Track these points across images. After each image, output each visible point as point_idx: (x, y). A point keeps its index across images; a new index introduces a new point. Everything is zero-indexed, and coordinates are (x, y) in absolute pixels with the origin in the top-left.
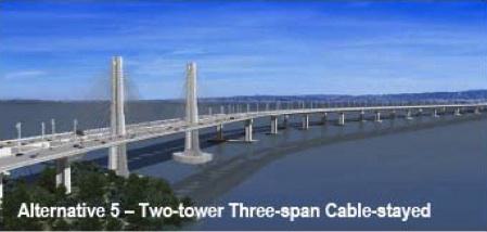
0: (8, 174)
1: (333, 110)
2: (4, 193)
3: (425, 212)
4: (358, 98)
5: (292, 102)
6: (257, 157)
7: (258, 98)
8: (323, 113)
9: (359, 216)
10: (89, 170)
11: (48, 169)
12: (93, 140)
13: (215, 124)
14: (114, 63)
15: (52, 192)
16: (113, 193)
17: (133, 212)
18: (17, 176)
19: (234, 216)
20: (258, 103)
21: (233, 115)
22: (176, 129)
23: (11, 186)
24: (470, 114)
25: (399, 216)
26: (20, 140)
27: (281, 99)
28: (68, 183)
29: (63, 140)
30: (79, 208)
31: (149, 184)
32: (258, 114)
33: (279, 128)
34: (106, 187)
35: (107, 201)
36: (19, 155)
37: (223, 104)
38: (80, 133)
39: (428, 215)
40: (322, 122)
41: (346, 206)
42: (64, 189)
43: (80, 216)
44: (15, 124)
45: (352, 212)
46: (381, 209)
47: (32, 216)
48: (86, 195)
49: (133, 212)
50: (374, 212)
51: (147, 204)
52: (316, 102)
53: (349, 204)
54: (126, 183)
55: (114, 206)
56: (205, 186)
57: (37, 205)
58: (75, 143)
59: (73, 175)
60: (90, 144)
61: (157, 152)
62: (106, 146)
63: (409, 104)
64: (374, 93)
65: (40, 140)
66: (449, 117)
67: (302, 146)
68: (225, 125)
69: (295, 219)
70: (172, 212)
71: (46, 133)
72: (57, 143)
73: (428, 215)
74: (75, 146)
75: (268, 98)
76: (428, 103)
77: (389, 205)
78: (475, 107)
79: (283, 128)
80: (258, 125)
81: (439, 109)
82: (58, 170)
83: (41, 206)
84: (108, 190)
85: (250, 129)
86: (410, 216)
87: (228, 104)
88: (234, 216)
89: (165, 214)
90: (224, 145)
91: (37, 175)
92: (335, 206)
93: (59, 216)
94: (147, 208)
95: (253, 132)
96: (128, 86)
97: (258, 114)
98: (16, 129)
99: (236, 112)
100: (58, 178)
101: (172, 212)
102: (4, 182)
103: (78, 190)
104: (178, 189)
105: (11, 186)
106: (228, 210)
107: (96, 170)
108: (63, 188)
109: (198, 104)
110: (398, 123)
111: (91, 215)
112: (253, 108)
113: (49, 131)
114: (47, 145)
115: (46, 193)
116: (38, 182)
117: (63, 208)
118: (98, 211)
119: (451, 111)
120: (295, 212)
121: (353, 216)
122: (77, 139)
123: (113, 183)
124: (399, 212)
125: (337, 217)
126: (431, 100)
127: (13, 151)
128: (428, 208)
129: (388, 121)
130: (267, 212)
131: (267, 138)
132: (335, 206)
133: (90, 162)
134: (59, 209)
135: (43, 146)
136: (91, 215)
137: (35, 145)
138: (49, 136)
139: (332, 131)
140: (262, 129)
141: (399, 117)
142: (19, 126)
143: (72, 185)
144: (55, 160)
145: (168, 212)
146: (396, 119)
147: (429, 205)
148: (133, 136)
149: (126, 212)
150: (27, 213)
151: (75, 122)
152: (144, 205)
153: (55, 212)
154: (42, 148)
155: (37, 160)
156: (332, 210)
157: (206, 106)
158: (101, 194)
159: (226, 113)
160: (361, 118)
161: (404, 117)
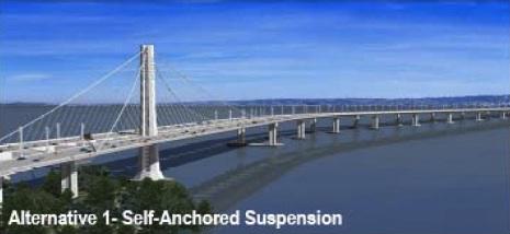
0: (8, 178)
2: (4, 197)
3: (234, 219)
4: (395, 101)
6: (282, 161)
8: (355, 116)
9: (215, 223)
10: (98, 174)
11: (52, 173)
12: (108, 143)
13: (236, 128)
15: (58, 196)
16: (124, 196)
18: (19, 181)
20: (283, 106)
21: (256, 119)
23: (12, 191)
24: (496, 120)
29: (70, 144)
30: (70, 215)
32: (283, 117)
33: (380, 125)
35: (118, 206)
36: (21, 159)
38: (88, 137)
40: (353, 126)
46: (312, 217)
47: (23, 223)
48: (94, 199)
53: (194, 212)
56: (152, 196)
58: (84, 146)
61: (172, 156)
63: (451, 108)
65: (44, 145)
66: (468, 124)
67: (332, 150)
69: (281, 226)
71: (51, 137)
72: (63, 147)
73: (237, 223)
74: (83, 150)
75: (294, 101)
76: (471, 107)
79: (310, 132)
82: (64, 173)
83: (32, 213)
84: (118, 194)
85: (273, 134)
87: (258, 108)
90: (244, 149)
91: (39, 179)
93: (49, 223)
95: (278, 137)
97: (283, 117)
99: (259, 115)
100: (64, 183)
102: (4, 187)
104: (196, 193)
105: (12, 191)
107: (105, 174)
108: (69, 192)
109: (159, 108)
110: (439, 127)
111: (83, 222)
112: (278, 111)
114: (52, 149)
115: (51, 198)
116: (40, 189)
117: (54, 216)
122: (85, 144)
123: (124, 188)
126: (475, 104)
127: (14, 155)
130: (289, 219)
131: (294, 142)
133: (100, 166)
134: (50, 216)
138: (53, 140)
139: (364, 135)
140: (287, 133)
141: (493, 116)
143: (80, 190)
144: (62, 165)
145: (208, 219)
146: (436, 123)
147: (238, 212)
148: (204, 131)
150: (17, 221)
151: (83, 127)
154: (49, 151)
157: (168, 113)
158: (111, 198)
160: (432, 120)
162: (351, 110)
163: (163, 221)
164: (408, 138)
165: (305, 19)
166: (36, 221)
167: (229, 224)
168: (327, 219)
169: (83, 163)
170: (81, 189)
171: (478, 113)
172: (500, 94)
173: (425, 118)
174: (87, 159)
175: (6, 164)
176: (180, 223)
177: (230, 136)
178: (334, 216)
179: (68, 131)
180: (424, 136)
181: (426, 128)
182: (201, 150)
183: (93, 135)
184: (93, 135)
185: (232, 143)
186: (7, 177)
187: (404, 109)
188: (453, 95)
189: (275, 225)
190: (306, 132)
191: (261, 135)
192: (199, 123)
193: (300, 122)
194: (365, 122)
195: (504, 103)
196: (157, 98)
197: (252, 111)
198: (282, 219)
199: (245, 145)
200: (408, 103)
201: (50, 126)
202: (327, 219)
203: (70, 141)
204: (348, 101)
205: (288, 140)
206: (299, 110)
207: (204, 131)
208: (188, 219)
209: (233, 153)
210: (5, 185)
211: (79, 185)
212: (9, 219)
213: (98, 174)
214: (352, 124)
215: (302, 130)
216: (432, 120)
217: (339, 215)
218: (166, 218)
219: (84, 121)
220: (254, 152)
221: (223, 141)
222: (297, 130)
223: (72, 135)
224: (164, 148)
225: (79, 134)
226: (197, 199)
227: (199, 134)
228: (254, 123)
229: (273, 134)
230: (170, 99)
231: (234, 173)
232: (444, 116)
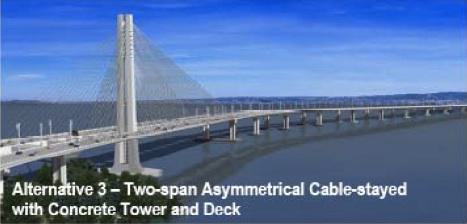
4: (336, 99)
5: (252, 103)
7: (242, 99)
11: (45, 166)
12: (90, 139)
17: (118, 190)
19: (129, 193)
22: (165, 129)
25: (378, 194)
26: (19, 140)
27: (262, 100)
29: (61, 139)
33: (291, 124)
36: (18, 153)
37: (209, 105)
38: (75, 133)
39: (405, 193)
41: (328, 185)
43: (270, 194)
44: (15, 124)
45: (334, 190)
49: (118, 190)
50: (354, 190)
51: (132, 183)
53: (331, 184)
57: (30, 184)
60: (83, 143)
62: (113, 141)
65: (38, 140)
69: (174, 197)
70: (155, 190)
71: (44, 134)
73: (405, 193)
75: (251, 99)
78: (444, 108)
81: (410, 110)
86: (387, 194)
88: (129, 193)
90: (212, 146)
92: (318, 185)
94: (131, 186)
95: (237, 133)
98: (16, 131)
100: (55, 177)
101: (155, 190)
107: (90, 167)
109: (137, 103)
110: (373, 123)
111: (80, 193)
113: (46, 132)
114: (45, 144)
118: (88, 190)
120: (174, 190)
121: (335, 194)
122: (73, 139)
124: (377, 190)
125: (320, 195)
126: (403, 101)
127: (13, 149)
128: (404, 187)
132: (318, 185)
133: (85, 159)
134: (50, 188)
137: (34, 143)
139: (310, 131)
140: (245, 129)
142: (18, 126)
144: (53, 158)
147: (405, 184)
148: (173, 127)
149: (113, 190)
150: (20, 192)
153: (47, 190)
154: (42, 146)
156: (315, 189)
157: (146, 111)
161: (349, 120)
165: (234, 26)
167: (397, 194)
175: (5, 159)
176: (280, 194)
177: (196, 132)
179: (59, 128)
180: (389, 128)
181: (330, 128)
182: (163, 147)
184: (79, 132)
185: (198, 139)
186: (7, 171)
187: (344, 106)
188: (384, 94)
189: (169, 195)
190: (261, 129)
191: (221, 132)
193: (255, 119)
195: (427, 101)
196: (137, 97)
197: (197, 110)
198: (174, 190)
199: (207, 140)
206: (256, 107)
207: (173, 127)
209: (200, 147)
210: (5, 178)
211: (68, 177)
212: (12, 191)
213: (84, 167)
215: (257, 125)
216: (338, 119)
217: (194, 187)
218: (207, 189)
219: (72, 118)
220: (216, 148)
221: (190, 137)
222: (253, 127)
224: (145, 142)
225: (68, 131)
227: (169, 131)
229: (233, 131)
230: (157, 94)
231: (199, 166)
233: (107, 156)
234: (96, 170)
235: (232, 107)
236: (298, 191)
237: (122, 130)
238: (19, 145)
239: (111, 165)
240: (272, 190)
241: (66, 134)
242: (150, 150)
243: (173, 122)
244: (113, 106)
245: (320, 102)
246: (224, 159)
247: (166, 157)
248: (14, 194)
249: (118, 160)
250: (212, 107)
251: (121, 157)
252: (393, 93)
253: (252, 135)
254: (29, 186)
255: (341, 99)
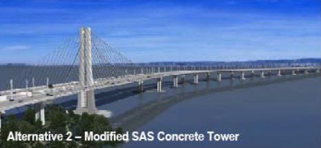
1: (190, 72)
3: (125, 137)
7: (165, 63)
8: (207, 73)
11: (30, 109)
12: (62, 90)
14: (83, 32)
16: (72, 124)
19: (211, 139)
24: (302, 74)
26: (13, 91)
28: (43, 119)
29: (40, 91)
30: (46, 135)
31: (95, 118)
32: (166, 74)
34: (67, 122)
38: (51, 86)
40: (206, 79)
42: (41, 122)
43: (46, 140)
47: (16, 140)
51: (213, 132)
52: (202, 66)
54: (80, 119)
55: (69, 133)
59: (46, 114)
60: (58, 93)
63: (263, 67)
64: (240, 60)
66: (288, 76)
67: (194, 94)
68: (144, 81)
74: (48, 95)
75: (171, 63)
77: (196, 133)
80: (165, 80)
81: (296, 70)
85: (159, 84)
88: (211, 139)
89: (215, 138)
91: (23, 113)
92: (163, 133)
93: (33, 139)
96: (95, 49)
97: (166, 74)
100: (37, 115)
102: (2, 118)
103: (49, 123)
106: (207, 136)
107: (61, 110)
108: (40, 122)
109: (93, 67)
110: (256, 80)
111: (54, 139)
112: (162, 70)
113: (30, 85)
114: (30, 94)
115: (28, 125)
116: (24, 118)
119: (290, 72)
123: (72, 119)
126: (276, 65)
127: (8, 98)
129: (249, 79)
132: (163, 133)
133: (57, 105)
134: (33, 135)
135: (27, 95)
136: (54, 139)
138: (31, 88)
140: (168, 83)
142: (11, 81)
146: (234, 79)
147: (127, 133)
148: (119, 82)
150: (13, 138)
151: (48, 80)
152: (210, 133)
153: (31, 137)
154: (26, 96)
155: (120, 84)
156: (162, 136)
157: (100, 71)
158: (64, 125)
159: (145, 73)
162: (205, 69)
163: (141, 138)
164: (238, 87)
165: (179, 11)
166: (232, 138)
168: (97, 137)
169: (48, 103)
170: (46, 119)
171: (293, 70)
172: (291, 59)
173: (267, 73)
174: (48, 100)
176: (177, 140)
178: (173, 135)
180: (248, 85)
183: (54, 85)
184: (54, 85)
185: (134, 90)
186: (3, 112)
192: (116, 77)
194: (188, 79)
196: (93, 61)
197: (134, 71)
198: (103, 137)
199: (143, 91)
200: (237, 65)
201: (28, 79)
202: (97, 137)
203: (40, 89)
204: (201, 63)
205: (169, 89)
208: (182, 137)
209: (137, 96)
210: (3, 117)
211: (45, 117)
212: (7, 137)
214: (205, 78)
215: (176, 81)
221: (129, 89)
222: (173, 82)
223: (41, 85)
225: (45, 84)
226: (115, 125)
227: (116, 84)
228: (148, 77)
229: (159, 84)
232: (237, 75)
233: (73, 102)
234: (65, 112)
235: (159, 68)
236: (198, 137)
237: (83, 83)
238: (12, 95)
239: (75, 108)
240: (48, 137)
241: (44, 86)
242: (103, 98)
243: (119, 78)
244: (77, 68)
245: (219, 65)
246: (154, 104)
247: (112, 103)
248: (8, 140)
249: (80, 105)
250: (145, 68)
251: (82, 102)
252: (277, 59)
253: (171, 87)
254: (18, 134)
255: (234, 63)
